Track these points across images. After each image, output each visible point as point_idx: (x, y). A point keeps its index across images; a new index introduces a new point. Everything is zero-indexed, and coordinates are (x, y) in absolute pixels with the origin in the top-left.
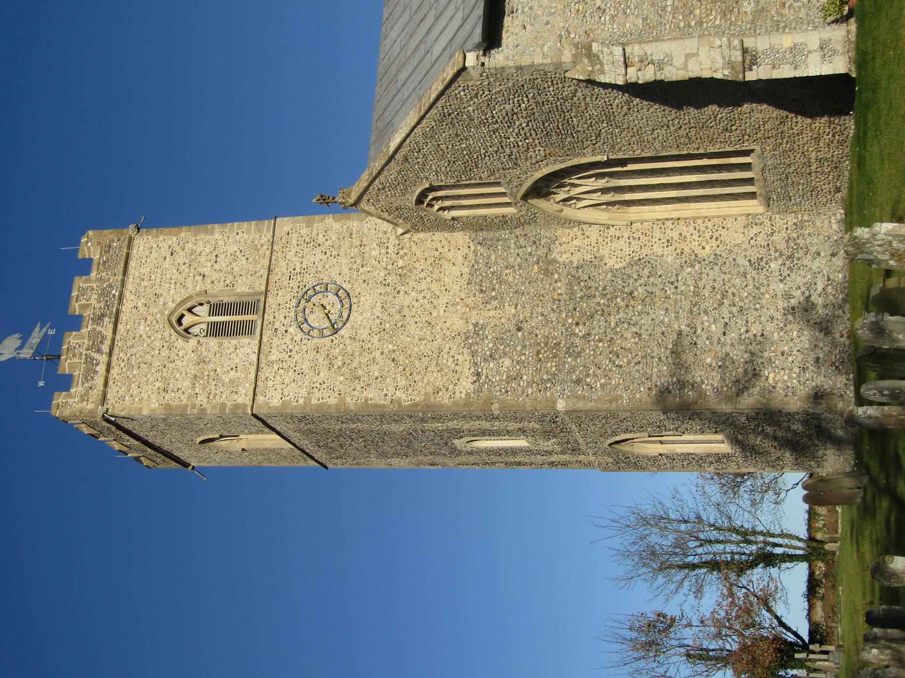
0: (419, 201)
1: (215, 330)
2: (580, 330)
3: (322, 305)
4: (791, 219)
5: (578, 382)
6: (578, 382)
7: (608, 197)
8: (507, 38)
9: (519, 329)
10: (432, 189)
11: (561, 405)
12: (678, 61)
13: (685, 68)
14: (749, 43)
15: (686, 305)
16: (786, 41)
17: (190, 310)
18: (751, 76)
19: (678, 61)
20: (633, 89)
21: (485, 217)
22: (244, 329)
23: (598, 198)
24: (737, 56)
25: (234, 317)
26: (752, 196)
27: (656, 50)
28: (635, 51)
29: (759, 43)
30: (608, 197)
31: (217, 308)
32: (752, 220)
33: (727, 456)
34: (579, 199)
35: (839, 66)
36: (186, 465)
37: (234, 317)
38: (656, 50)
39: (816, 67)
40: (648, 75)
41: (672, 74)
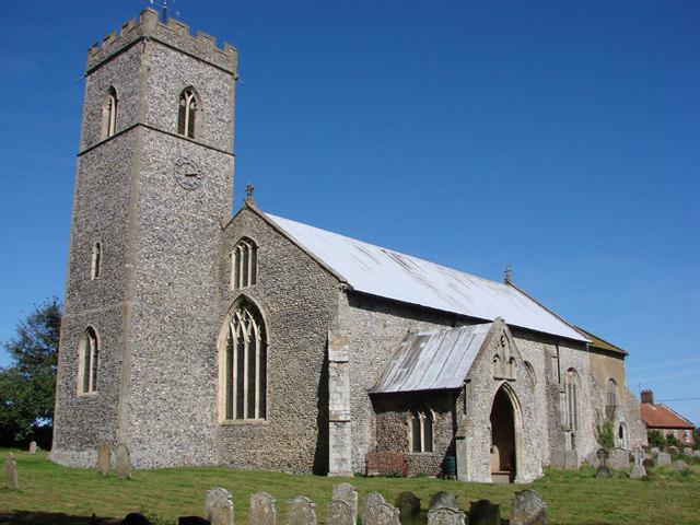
0: (245, 238)
1: (182, 110)
2: (167, 318)
3: (526, 363)
4: (213, 437)
5: (141, 315)
6: (141, 315)
7: (236, 342)
8: (353, 311)
10: (255, 248)
11: (131, 304)
12: (339, 389)
13: (336, 392)
15: (176, 378)
16: (348, 441)
18: (331, 425)
19: (339, 389)
20: (326, 362)
21: (230, 272)
22: (181, 130)
23: (236, 335)
24: (342, 418)
25: (187, 125)
26: (230, 416)
27: (345, 378)
28: (344, 367)
29: (347, 429)
30: (236, 342)
31: (192, 113)
32: (215, 416)
33: (73, 394)
34: (236, 325)
35: (333, 467)
36: (90, 72)
37: (187, 125)
38: (345, 378)
39: (333, 455)
40: (332, 373)
41: (332, 385)
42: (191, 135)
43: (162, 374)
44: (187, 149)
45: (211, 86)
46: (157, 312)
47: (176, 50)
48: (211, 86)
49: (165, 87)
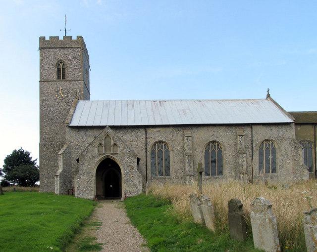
1: (59, 70)
14: (59, 177)
17: (64, 64)
42: (64, 78)
44: (61, 85)
45: (70, 57)
47: (52, 48)
49: (49, 65)
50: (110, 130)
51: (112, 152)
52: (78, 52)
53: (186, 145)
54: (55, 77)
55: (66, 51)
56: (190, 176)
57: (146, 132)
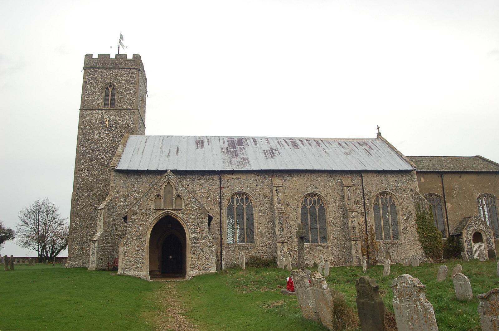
1: (107, 96)
6: (80, 197)
9: (97, 180)
31: (113, 96)
43: (91, 224)
45: (123, 79)
46: (88, 195)
48: (123, 79)
49: (95, 88)
50: (172, 177)
51: (174, 207)
52: (133, 73)
53: (275, 197)
54: (101, 103)
55: (117, 73)
56: (283, 243)
57: (220, 179)
